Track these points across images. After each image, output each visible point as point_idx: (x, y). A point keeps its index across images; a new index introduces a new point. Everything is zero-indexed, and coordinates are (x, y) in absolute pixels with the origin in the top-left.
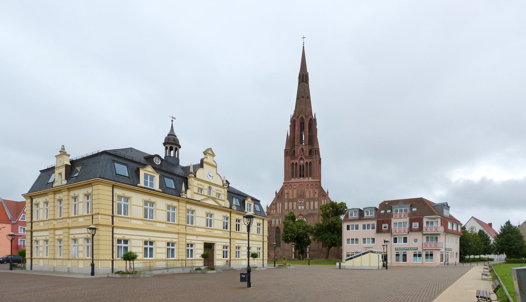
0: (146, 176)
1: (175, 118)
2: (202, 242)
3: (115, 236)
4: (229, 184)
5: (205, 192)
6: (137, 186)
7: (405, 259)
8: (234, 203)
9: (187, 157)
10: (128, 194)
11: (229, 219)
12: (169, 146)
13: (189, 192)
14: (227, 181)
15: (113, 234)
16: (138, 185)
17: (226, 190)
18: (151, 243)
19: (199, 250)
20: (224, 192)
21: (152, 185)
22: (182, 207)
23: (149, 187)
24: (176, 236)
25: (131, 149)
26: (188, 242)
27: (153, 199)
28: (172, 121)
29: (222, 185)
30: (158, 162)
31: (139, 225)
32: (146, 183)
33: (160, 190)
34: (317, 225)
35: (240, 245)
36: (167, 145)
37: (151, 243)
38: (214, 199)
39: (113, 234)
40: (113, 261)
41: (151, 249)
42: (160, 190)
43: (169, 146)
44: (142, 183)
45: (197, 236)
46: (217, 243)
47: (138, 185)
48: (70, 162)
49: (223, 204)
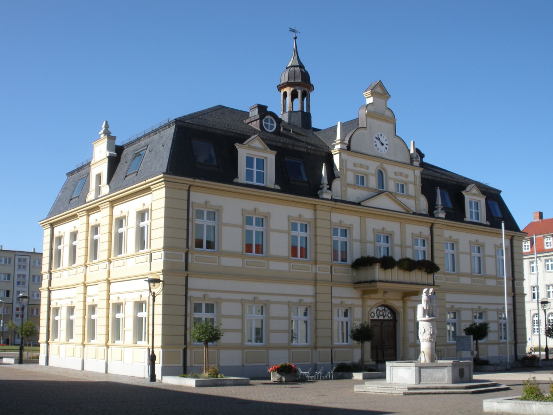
3: (190, 293)
4: (422, 156)
5: (373, 182)
7: (24, 276)
8: (439, 201)
9: (328, 113)
11: (428, 243)
12: (289, 90)
13: (336, 184)
14: (417, 151)
17: (418, 172)
20: (413, 176)
21: (260, 177)
23: (255, 183)
25: (220, 109)
27: (264, 207)
29: (408, 161)
32: (249, 174)
33: (278, 187)
34: (220, 334)
35: (483, 307)
36: (285, 90)
38: (392, 195)
43: (289, 90)
48: (116, 151)
49: (411, 204)
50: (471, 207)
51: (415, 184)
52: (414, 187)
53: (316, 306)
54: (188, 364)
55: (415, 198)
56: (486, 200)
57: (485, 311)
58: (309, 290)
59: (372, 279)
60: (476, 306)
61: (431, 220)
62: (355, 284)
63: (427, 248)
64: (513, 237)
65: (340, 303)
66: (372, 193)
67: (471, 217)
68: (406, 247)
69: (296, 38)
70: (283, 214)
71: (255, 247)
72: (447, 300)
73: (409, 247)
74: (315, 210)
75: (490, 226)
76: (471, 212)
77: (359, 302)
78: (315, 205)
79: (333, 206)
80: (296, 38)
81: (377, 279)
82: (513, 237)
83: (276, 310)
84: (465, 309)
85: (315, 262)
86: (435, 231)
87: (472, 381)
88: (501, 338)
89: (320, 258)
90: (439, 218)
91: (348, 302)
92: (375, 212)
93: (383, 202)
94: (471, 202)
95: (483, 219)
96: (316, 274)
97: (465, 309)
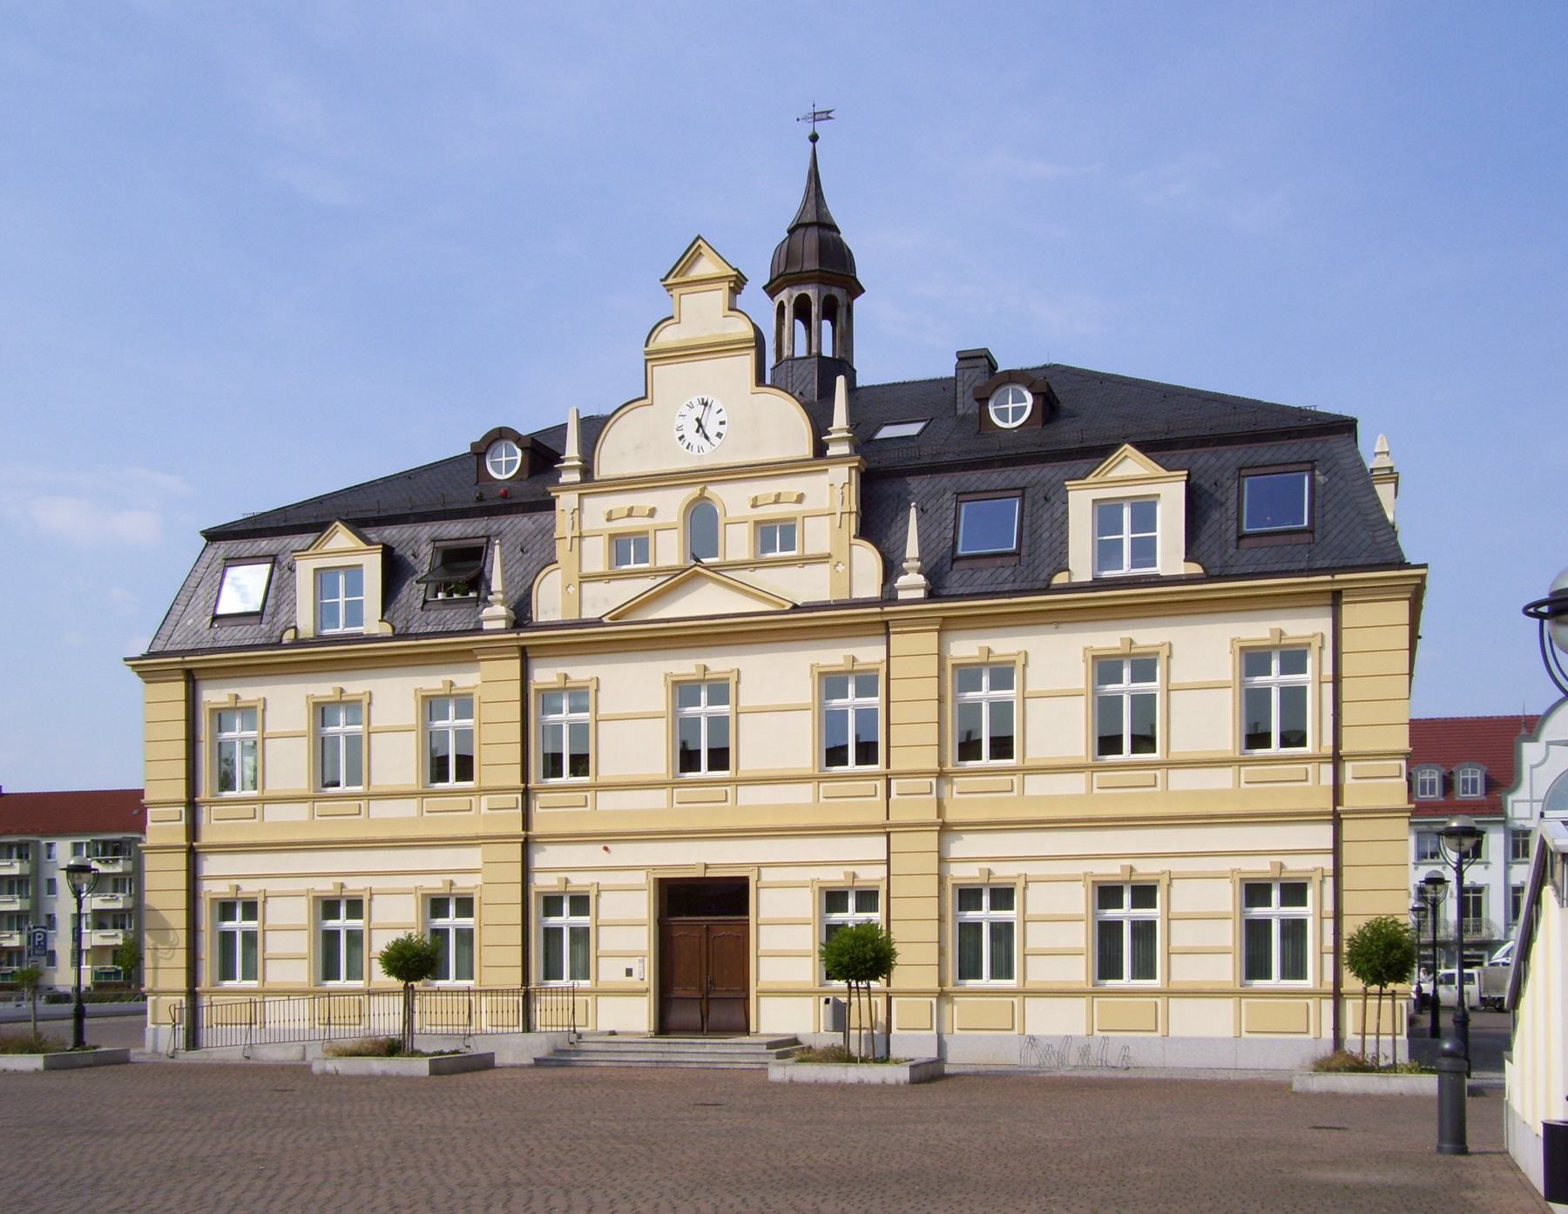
0: (1107, 515)
1: (826, 115)
2: (641, 878)
6: (1048, 589)
10: (1004, 645)
15: (1337, 852)
16: (1060, 579)
18: (1145, 895)
19: (626, 937)
22: (490, 683)
24: (874, 847)
26: (964, 873)
28: (814, 138)
30: (1002, 415)
31: (294, 825)
33: (1196, 569)
37: (1145, 895)
39: (1337, 852)
40: (527, 997)
41: (1145, 932)
42: (1196, 569)
44: (1081, 564)
45: (606, 839)
46: (768, 875)
47: (1060, 579)
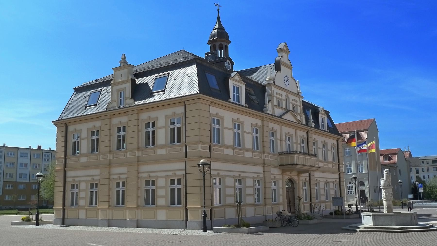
27: (242, 118)
35: (243, 175)
50: (234, 92)
51: (300, 107)
52: (299, 110)
53: (265, 179)
54: (66, 217)
55: (300, 115)
56: (246, 86)
57: (244, 178)
58: (260, 169)
59: (293, 163)
60: (237, 174)
61: (308, 128)
62: (280, 165)
63: (305, 145)
64: (338, 139)
65: (257, 176)
66: (284, 111)
67: (234, 100)
68: (283, 141)
69: (218, 10)
70: (249, 121)
71: (239, 140)
72: (272, 173)
73: (320, 148)
74: (262, 120)
75: (329, 132)
76: (234, 95)
77: (280, 177)
78: (263, 117)
79: (213, 101)
80: (218, 10)
81: (296, 163)
82: (338, 139)
83: (249, 182)
84: (249, 178)
85: (264, 153)
86: (309, 134)
87: (418, 225)
88: (256, 202)
89: (266, 150)
90: (312, 127)
91: (277, 177)
92: (223, 104)
93: (289, 117)
94: (234, 87)
95: (243, 101)
96: (264, 159)
97: (249, 178)
